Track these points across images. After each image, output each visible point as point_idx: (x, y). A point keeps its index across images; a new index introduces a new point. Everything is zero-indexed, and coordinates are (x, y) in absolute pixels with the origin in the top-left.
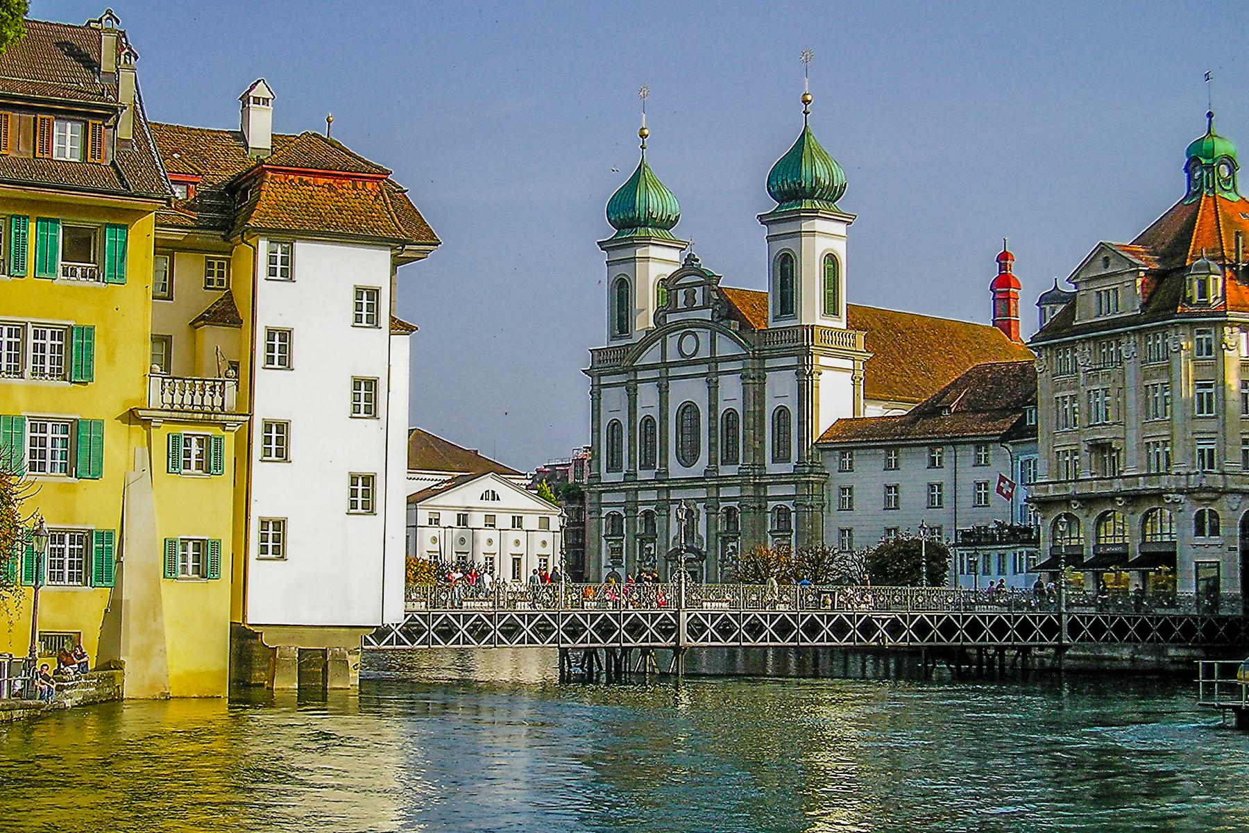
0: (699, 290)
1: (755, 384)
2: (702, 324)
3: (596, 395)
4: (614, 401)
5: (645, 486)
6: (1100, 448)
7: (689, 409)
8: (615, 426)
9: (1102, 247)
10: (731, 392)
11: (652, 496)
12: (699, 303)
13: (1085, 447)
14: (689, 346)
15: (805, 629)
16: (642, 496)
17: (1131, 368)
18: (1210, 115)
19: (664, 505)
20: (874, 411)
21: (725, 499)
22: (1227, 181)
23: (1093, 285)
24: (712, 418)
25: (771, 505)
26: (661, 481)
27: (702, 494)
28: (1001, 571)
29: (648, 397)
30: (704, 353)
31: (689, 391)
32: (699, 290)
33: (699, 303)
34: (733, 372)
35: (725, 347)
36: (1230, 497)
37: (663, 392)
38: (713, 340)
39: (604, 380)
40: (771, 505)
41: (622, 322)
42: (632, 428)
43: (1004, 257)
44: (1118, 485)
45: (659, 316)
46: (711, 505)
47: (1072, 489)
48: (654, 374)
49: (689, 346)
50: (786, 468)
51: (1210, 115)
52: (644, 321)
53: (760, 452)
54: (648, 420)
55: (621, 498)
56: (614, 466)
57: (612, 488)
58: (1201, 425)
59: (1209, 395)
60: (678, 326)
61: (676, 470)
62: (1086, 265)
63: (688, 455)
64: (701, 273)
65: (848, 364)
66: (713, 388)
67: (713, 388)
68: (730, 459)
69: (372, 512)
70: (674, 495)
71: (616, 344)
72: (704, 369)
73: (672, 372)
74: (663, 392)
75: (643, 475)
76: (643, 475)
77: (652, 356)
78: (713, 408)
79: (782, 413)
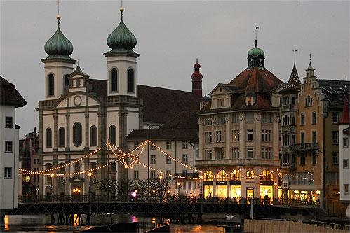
0: (82, 81)
1: (103, 115)
2: (82, 93)
3: (41, 118)
6: (217, 150)
7: (77, 126)
8: (49, 131)
9: (219, 85)
10: (94, 120)
11: (64, 157)
12: (82, 85)
13: (213, 149)
14: (78, 101)
15: (62, 209)
16: (59, 157)
17: (228, 125)
18: (256, 41)
20: (146, 127)
21: (92, 159)
22: (260, 63)
23: (217, 97)
24: (87, 129)
25: (91, 161)
26: (67, 152)
28: (190, 188)
29: (62, 120)
30: (84, 104)
32: (82, 81)
33: (82, 85)
34: (95, 112)
35: (92, 102)
36: (256, 167)
37: (68, 118)
38: (87, 99)
39: (44, 113)
40: (45, 163)
41: (51, 91)
42: (56, 131)
43: (197, 67)
44: (223, 162)
45: (65, 90)
47: (209, 163)
48: (65, 111)
49: (78, 101)
50: (50, 150)
51: (256, 41)
53: (103, 142)
54: (62, 129)
55: (51, 158)
56: (49, 145)
57: (48, 154)
58: (248, 144)
59: (251, 135)
60: (73, 93)
62: (215, 90)
63: (78, 141)
64: (82, 74)
65: (137, 110)
66: (87, 117)
67: (87, 117)
68: (93, 143)
69: (344, 160)
70: (72, 157)
71: (49, 99)
72: (84, 110)
73: (71, 111)
74: (68, 118)
75: (60, 149)
76: (60, 149)
77: (63, 104)
78: (87, 125)
79: (113, 128)
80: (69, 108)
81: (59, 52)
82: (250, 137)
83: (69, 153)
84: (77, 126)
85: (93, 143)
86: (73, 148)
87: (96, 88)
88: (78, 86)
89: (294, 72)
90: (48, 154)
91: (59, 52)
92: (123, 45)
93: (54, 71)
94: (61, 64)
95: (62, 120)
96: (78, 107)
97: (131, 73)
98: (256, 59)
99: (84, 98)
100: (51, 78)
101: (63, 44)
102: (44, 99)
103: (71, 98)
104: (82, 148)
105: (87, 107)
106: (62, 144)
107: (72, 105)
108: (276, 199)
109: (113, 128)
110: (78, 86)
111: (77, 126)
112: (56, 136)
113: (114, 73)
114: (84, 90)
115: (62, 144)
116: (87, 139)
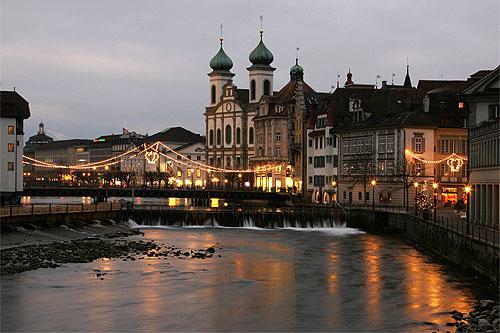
1: (245, 119)
2: (231, 100)
4: (211, 122)
5: (218, 150)
6: (260, 148)
8: (211, 131)
10: (239, 123)
19: (224, 155)
29: (219, 121)
31: (228, 121)
35: (238, 109)
37: (223, 121)
41: (214, 101)
45: (222, 98)
52: (218, 100)
53: (245, 141)
60: (226, 101)
61: (226, 146)
66: (235, 120)
67: (235, 120)
68: (238, 142)
74: (223, 121)
77: (219, 110)
80: (223, 113)
81: (222, 67)
82: (278, 139)
83: (223, 149)
84: (228, 126)
85: (238, 142)
86: (226, 146)
87: (241, 96)
88: (229, 95)
89: (408, 78)
90: (229, 150)
91: (222, 67)
92: (262, 61)
93: (255, 78)
94: (220, 77)
95: (219, 121)
96: (228, 112)
97: (267, 84)
98: (297, 74)
99: (232, 104)
100: (214, 88)
101: (264, 55)
102: (209, 105)
103: (225, 105)
104: (230, 146)
105: (235, 112)
106: (219, 143)
107: (225, 111)
108: (274, 189)
109: (251, 129)
110: (229, 95)
111: (228, 126)
113: (253, 83)
114: (233, 98)
115: (219, 143)
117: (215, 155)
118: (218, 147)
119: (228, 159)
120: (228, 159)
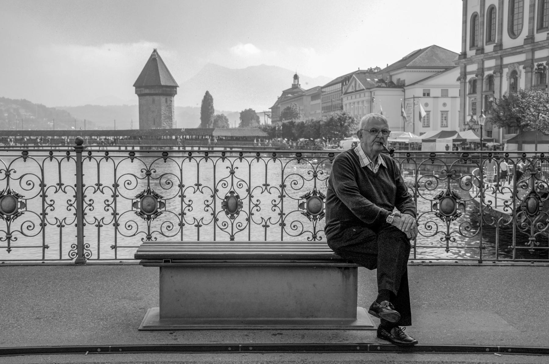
19: (499, 69)
27: (522, 58)
46: (528, 65)
68: (490, 40)
70: (507, 60)
90: (514, 51)
112: (501, 25)
116: (532, 19)
117: (482, 70)
118: (489, 48)
119: (514, 75)
120: (514, 75)
